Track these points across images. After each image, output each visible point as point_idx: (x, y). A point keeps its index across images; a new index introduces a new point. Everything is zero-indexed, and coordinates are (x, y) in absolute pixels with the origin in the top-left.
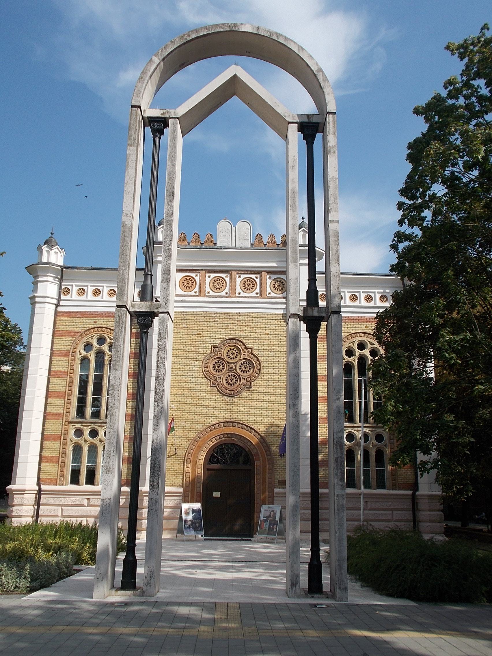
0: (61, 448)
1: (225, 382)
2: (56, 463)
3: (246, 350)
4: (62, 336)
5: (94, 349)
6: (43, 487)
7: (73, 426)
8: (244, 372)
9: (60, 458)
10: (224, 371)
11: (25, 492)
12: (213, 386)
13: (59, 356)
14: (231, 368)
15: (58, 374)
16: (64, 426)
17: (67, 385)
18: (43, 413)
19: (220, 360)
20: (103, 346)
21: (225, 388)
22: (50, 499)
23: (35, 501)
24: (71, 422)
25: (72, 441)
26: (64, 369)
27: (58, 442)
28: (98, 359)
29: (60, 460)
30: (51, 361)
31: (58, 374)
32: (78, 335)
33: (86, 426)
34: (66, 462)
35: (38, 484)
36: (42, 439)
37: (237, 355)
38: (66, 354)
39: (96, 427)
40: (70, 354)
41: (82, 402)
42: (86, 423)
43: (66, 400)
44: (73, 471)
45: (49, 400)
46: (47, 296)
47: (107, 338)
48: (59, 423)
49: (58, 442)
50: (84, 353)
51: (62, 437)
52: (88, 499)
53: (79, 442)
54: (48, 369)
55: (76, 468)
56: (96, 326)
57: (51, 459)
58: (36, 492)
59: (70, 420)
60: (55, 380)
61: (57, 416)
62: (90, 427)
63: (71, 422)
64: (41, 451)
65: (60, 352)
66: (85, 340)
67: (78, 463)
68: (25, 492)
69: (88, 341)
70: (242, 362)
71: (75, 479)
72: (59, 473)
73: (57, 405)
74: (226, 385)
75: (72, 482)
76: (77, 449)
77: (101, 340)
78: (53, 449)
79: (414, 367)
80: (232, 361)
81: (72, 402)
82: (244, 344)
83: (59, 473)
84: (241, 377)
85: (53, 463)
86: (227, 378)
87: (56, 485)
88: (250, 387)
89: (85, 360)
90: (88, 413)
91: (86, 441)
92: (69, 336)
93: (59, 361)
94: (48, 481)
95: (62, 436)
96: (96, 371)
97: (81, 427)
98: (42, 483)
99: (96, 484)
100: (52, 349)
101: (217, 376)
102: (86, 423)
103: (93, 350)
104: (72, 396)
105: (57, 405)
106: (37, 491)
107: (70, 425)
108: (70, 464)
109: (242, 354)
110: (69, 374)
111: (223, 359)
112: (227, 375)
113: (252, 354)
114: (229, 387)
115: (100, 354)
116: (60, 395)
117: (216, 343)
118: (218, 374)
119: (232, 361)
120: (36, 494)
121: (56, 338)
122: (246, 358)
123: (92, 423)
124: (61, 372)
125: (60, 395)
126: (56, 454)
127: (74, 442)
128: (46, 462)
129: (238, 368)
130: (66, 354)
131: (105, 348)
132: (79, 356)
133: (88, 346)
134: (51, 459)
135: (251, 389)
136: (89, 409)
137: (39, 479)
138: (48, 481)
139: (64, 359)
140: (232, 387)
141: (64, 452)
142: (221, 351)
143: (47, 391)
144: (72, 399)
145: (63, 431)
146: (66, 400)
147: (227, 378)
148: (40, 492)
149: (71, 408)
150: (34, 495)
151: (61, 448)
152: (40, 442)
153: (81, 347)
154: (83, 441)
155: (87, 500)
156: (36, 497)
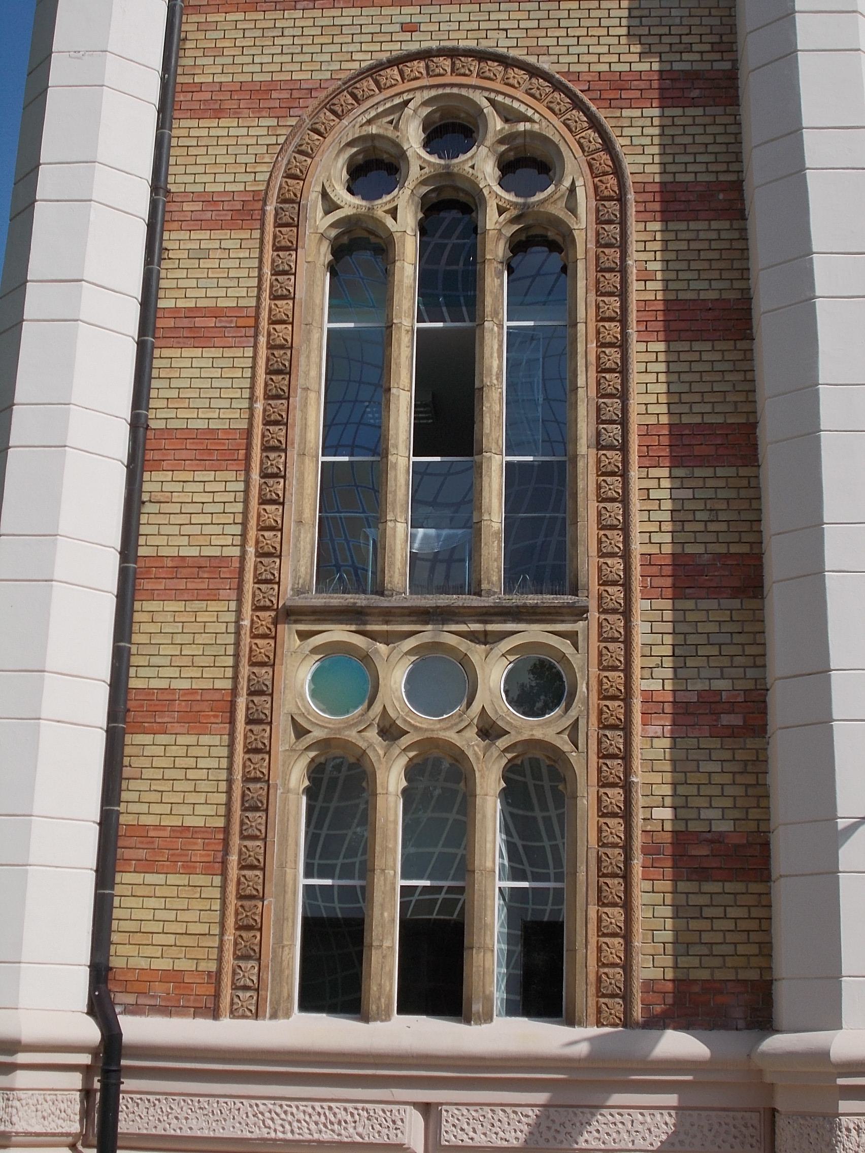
0: (238, 776)
2: (207, 871)
4: (218, 114)
5: (414, 173)
6: (135, 1029)
7: (304, 636)
9: (235, 840)
11: (22, 1058)
13: (200, 224)
15: (203, 328)
16: (246, 640)
17: (260, 391)
18: (147, 190)
20: (462, 158)
22: (180, 1108)
23: (86, 1114)
24: (290, 614)
25: (300, 732)
26: (223, 543)
27: (215, 741)
28: (436, 239)
29: (231, 849)
30: (154, 251)
31: (203, 328)
32: (313, 103)
33: (388, 638)
34: (273, 865)
35: (100, 1007)
36: (112, 716)
38: (244, 212)
39: (453, 640)
40: (270, 209)
41: (351, 498)
42: (388, 615)
43: (255, 475)
44: (314, 928)
45: (152, 482)
46: (81, 318)
47: (488, 110)
48: (216, 617)
49: (215, 741)
50: (351, 204)
51: (271, 214)
52: (426, 1109)
53: (351, 735)
54: (106, 675)
55: (338, 909)
56: (414, 47)
57: (173, 850)
58: (85, 1059)
59: (287, 595)
60: (179, 364)
61: (199, 576)
62: (409, 644)
63: (290, 614)
64: (121, 660)
65: (209, 200)
66: (352, 126)
67: (347, 872)
68: (22, 1058)
69: (373, 129)
71: (332, 980)
72: (229, 937)
73: (201, 513)
75: (314, 998)
76: (339, 784)
77: (451, 130)
78: (185, 782)
81: (293, 489)
83: (229, 937)
85: (189, 869)
87: (215, 1014)
89: (359, 252)
90: (398, 564)
91: (390, 731)
92: (258, 112)
93: (202, 255)
94: (159, 989)
95: (242, 702)
96: (428, 309)
97: (360, 641)
98: (122, 998)
99: (477, 1007)
100: (158, 184)
102: (388, 615)
103: (410, 184)
104: (293, 453)
105: (201, 513)
106: (94, 1051)
107: (288, 634)
108: (293, 883)
110: (264, 323)
115: (450, 211)
116: (210, 449)
120: (87, 1071)
121: (182, 127)
123: (425, 615)
124: (216, 313)
125: (210, 449)
126: (205, 813)
127: (317, 734)
128: (147, 866)
130: (244, 212)
131: (482, 166)
132: (319, 222)
133: (374, 168)
134: (173, 850)
136: (402, 537)
137: (100, 973)
138: (159, 989)
139: (231, 239)
141: (253, 798)
143: (138, 425)
144: (293, 473)
145: (245, 670)
146: (255, 475)
148: (109, 1064)
149: (290, 525)
150: (76, 1080)
151: (238, 776)
152: (99, 740)
153: (331, 170)
154: (373, 735)
155: (416, 1120)
156: (87, 1093)
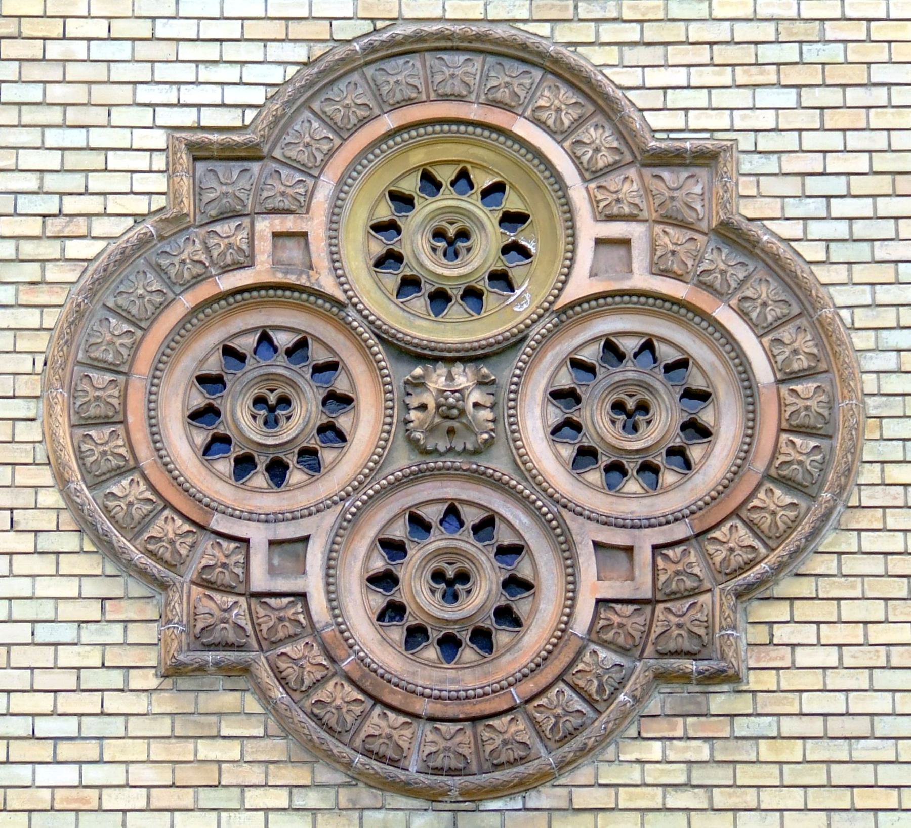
1: (360, 607)
3: (628, 186)
8: (300, 347)
10: (345, 466)
12: (204, 659)
14: (451, 414)
19: (286, 322)
21: (373, 690)
37: (512, 219)
57: (126, 681)
70: (584, 339)
74: (380, 648)
79: (73, 486)
80: (456, 330)
82: (598, 100)
84: (585, 535)
86: (393, 548)
88: (702, 670)
101: (259, 535)
109: (589, 229)
111: (335, 308)
112: (387, 518)
113: (733, 236)
114: (426, 671)
117: (236, 94)
118: (271, 502)
119: (456, 330)
122: (641, 279)
129: (535, 419)
134: (126, 681)
135: (719, 703)
140: (468, 675)
142: (303, 207)
147: (393, 548)
